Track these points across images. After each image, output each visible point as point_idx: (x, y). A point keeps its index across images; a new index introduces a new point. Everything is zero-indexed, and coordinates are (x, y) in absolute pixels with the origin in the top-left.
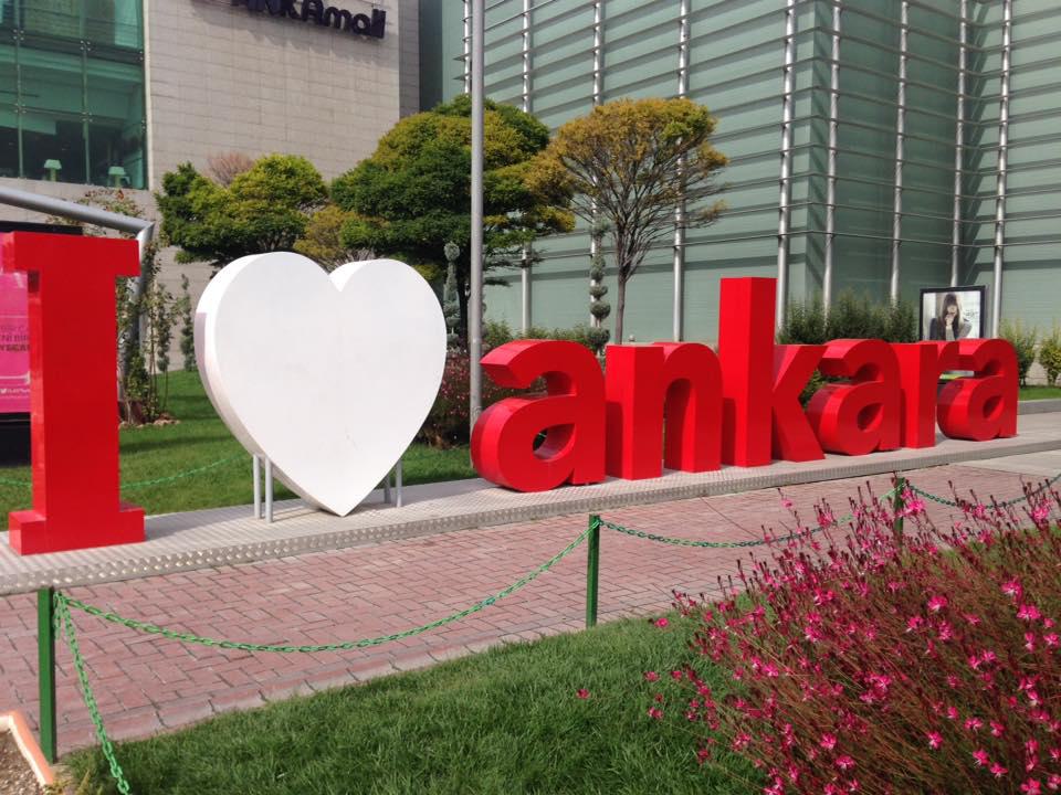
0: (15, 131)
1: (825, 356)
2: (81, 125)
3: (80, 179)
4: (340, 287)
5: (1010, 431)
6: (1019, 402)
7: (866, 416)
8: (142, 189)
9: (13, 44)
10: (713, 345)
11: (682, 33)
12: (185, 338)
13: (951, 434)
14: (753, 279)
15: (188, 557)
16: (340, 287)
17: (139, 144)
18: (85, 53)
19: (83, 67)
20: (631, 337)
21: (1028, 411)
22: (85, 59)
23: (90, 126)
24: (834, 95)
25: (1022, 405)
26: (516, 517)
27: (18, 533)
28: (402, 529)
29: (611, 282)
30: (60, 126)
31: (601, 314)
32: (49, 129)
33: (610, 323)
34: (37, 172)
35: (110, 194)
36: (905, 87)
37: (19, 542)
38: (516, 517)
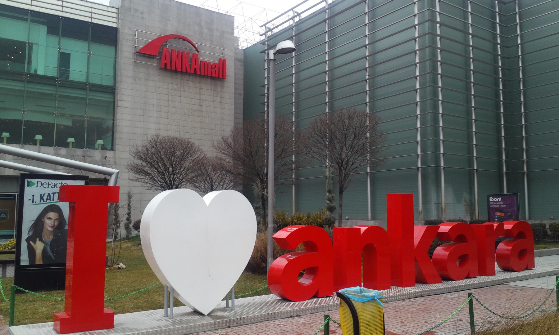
0: (53, 124)
1: (439, 231)
2: (84, 121)
3: (82, 147)
4: (208, 203)
5: (530, 266)
6: (535, 251)
7: (463, 259)
8: (110, 150)
9: (55, 85)
10: (385, 227)
11: (367, 74)
12: (127, 222)
13: (506, 269)
14: (403, 195)
15: (302, 312)
16: (208, 203)
17: (112, 130)
18: (88, 89)
19: (86, 95)
20: (347, 217)
21: (541, 255)
22: (88, 91)
23: (88, 121)
24: (498, 24)
25: (536, 252)
26: (323, 309)
27: (58, 323)
28: (252, 318)
29: (336, 195)
30: (74, 122)
31: (331, 209)
32: (69, 123)
33: (336, 215)
34: (62, 143)
35: (97, 154)
36: (474, 97)
37: (58, 328)
38: (323, 309)
